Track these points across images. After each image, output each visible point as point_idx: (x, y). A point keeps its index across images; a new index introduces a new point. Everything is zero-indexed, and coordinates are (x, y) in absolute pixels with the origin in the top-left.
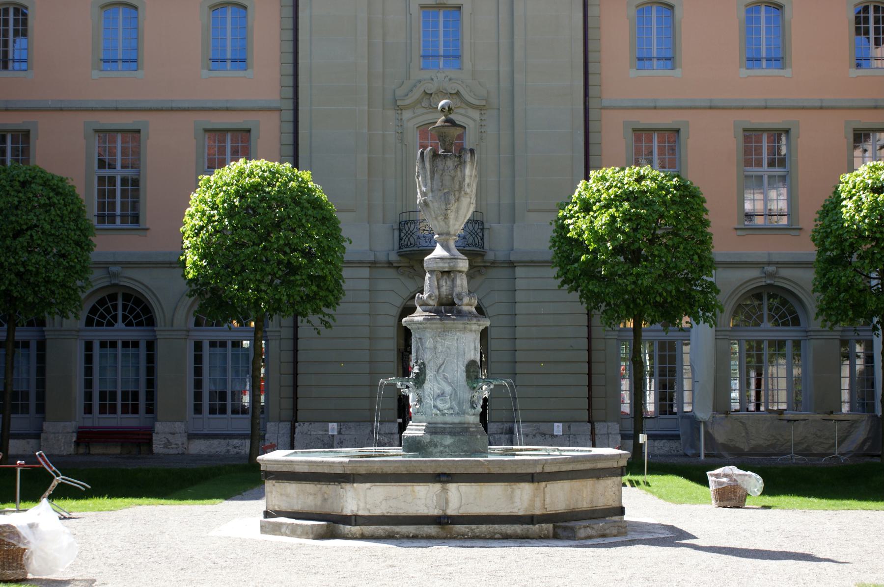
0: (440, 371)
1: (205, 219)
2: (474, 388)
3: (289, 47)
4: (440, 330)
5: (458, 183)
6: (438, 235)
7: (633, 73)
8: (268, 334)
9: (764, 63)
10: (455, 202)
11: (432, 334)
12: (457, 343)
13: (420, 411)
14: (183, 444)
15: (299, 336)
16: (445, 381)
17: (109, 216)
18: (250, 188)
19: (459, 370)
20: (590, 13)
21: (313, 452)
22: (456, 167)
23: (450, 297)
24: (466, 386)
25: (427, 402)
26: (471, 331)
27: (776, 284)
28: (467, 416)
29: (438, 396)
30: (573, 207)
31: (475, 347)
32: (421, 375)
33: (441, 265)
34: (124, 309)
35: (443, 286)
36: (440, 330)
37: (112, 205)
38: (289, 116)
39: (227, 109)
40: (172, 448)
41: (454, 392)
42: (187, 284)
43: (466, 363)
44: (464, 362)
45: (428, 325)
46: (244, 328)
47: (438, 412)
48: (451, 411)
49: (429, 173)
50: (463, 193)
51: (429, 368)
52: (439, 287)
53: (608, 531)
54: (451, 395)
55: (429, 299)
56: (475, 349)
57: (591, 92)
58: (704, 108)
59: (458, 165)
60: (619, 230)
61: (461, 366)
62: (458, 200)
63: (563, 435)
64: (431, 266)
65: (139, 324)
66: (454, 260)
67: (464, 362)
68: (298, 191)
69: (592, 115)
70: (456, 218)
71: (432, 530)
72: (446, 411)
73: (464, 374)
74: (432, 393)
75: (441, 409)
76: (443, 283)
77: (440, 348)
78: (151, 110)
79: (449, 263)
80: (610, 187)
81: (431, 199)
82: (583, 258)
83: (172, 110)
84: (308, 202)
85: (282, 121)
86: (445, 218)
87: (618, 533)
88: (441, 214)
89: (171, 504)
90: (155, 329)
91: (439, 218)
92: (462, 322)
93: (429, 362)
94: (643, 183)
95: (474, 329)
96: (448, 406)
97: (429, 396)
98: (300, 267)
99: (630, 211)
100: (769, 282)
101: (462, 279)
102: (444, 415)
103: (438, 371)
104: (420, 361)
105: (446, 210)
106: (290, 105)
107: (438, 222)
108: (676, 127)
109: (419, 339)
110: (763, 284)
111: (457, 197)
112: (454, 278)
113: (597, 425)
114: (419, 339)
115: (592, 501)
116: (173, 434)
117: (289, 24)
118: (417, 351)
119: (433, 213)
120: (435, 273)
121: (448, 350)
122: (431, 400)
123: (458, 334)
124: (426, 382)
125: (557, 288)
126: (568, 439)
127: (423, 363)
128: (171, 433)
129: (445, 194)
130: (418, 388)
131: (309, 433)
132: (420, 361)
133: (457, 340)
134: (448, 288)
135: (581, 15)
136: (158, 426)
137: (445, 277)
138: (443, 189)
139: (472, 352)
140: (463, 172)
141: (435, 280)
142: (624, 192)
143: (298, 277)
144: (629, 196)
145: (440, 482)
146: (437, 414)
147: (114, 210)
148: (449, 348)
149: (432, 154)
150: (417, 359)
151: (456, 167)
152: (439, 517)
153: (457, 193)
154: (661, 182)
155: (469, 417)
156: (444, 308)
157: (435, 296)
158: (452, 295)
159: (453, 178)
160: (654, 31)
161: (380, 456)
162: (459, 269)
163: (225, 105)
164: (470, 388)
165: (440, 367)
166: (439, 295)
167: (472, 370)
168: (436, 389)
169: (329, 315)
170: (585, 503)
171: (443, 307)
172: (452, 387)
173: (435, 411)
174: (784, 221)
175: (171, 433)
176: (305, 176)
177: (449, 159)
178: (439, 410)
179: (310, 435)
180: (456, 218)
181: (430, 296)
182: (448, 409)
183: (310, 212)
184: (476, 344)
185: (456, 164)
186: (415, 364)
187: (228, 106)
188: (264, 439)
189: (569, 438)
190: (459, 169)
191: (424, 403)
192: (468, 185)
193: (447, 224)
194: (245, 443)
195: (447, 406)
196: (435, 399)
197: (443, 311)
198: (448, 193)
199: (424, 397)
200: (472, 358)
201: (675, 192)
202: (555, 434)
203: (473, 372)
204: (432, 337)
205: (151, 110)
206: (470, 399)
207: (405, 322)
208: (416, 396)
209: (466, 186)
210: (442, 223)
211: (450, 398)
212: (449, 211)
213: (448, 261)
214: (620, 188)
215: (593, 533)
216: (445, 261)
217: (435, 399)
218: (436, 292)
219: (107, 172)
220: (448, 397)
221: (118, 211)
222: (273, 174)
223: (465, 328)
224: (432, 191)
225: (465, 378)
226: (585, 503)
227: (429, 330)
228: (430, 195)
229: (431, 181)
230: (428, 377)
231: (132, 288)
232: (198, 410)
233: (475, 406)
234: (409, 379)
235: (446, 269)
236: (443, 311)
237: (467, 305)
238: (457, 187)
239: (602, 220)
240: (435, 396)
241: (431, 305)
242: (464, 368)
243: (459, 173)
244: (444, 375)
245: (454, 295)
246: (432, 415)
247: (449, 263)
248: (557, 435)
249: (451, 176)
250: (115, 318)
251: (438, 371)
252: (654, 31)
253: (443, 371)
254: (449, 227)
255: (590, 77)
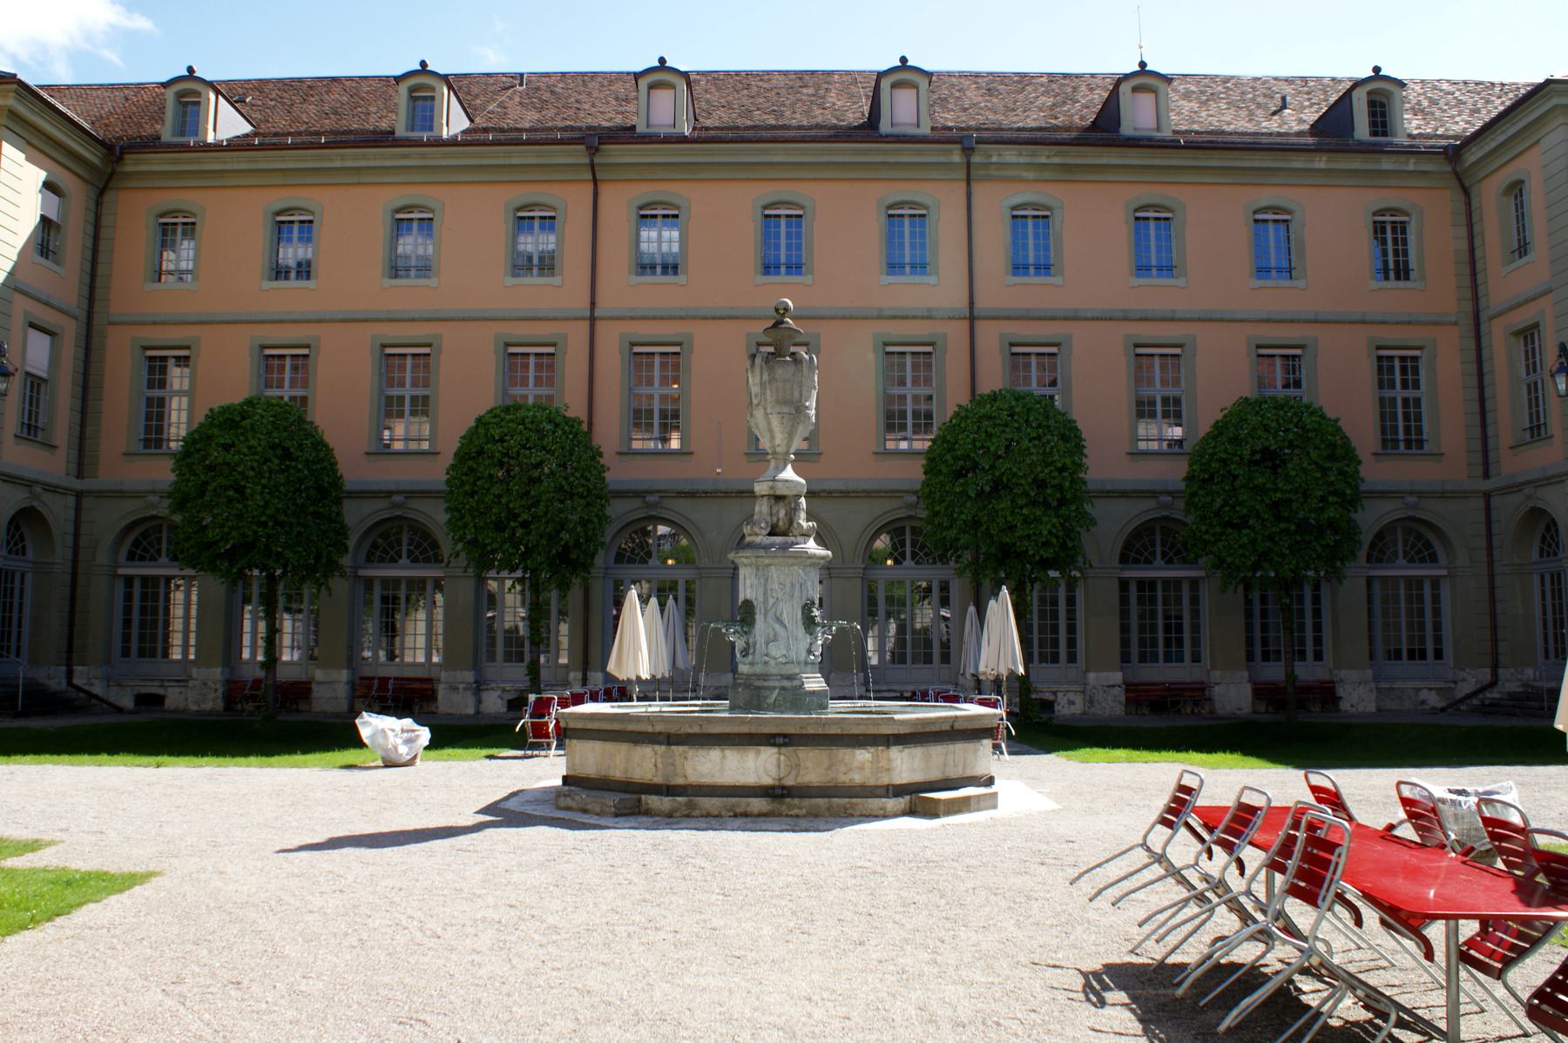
9: (1154, 272)
17: (1417, 441)
21: (922, 706)
27: (405, 515)
34: (1405, 545)
37: (1395, 430)
46: (899, 566)
53: (589, 807)
58: (923, 318)
71: (758, 804)
87: (602, 811)
89: (201, 766)
100: (1164, 514)
108: (932, 340)
110: (1158, 516)
115: (626, 771)
145: (774, 745)
147: (1397, 434)
152: (773, 787)
160: (907, 235)
161: (879, 713)
163: (531, 314)
170: (618, 772)
174: (425, 446)
215: (574, 805)
219: (897, 391)
221: (1401, 436)
226: (618, 772)
250: (1153, 554)
252: (907, 235)
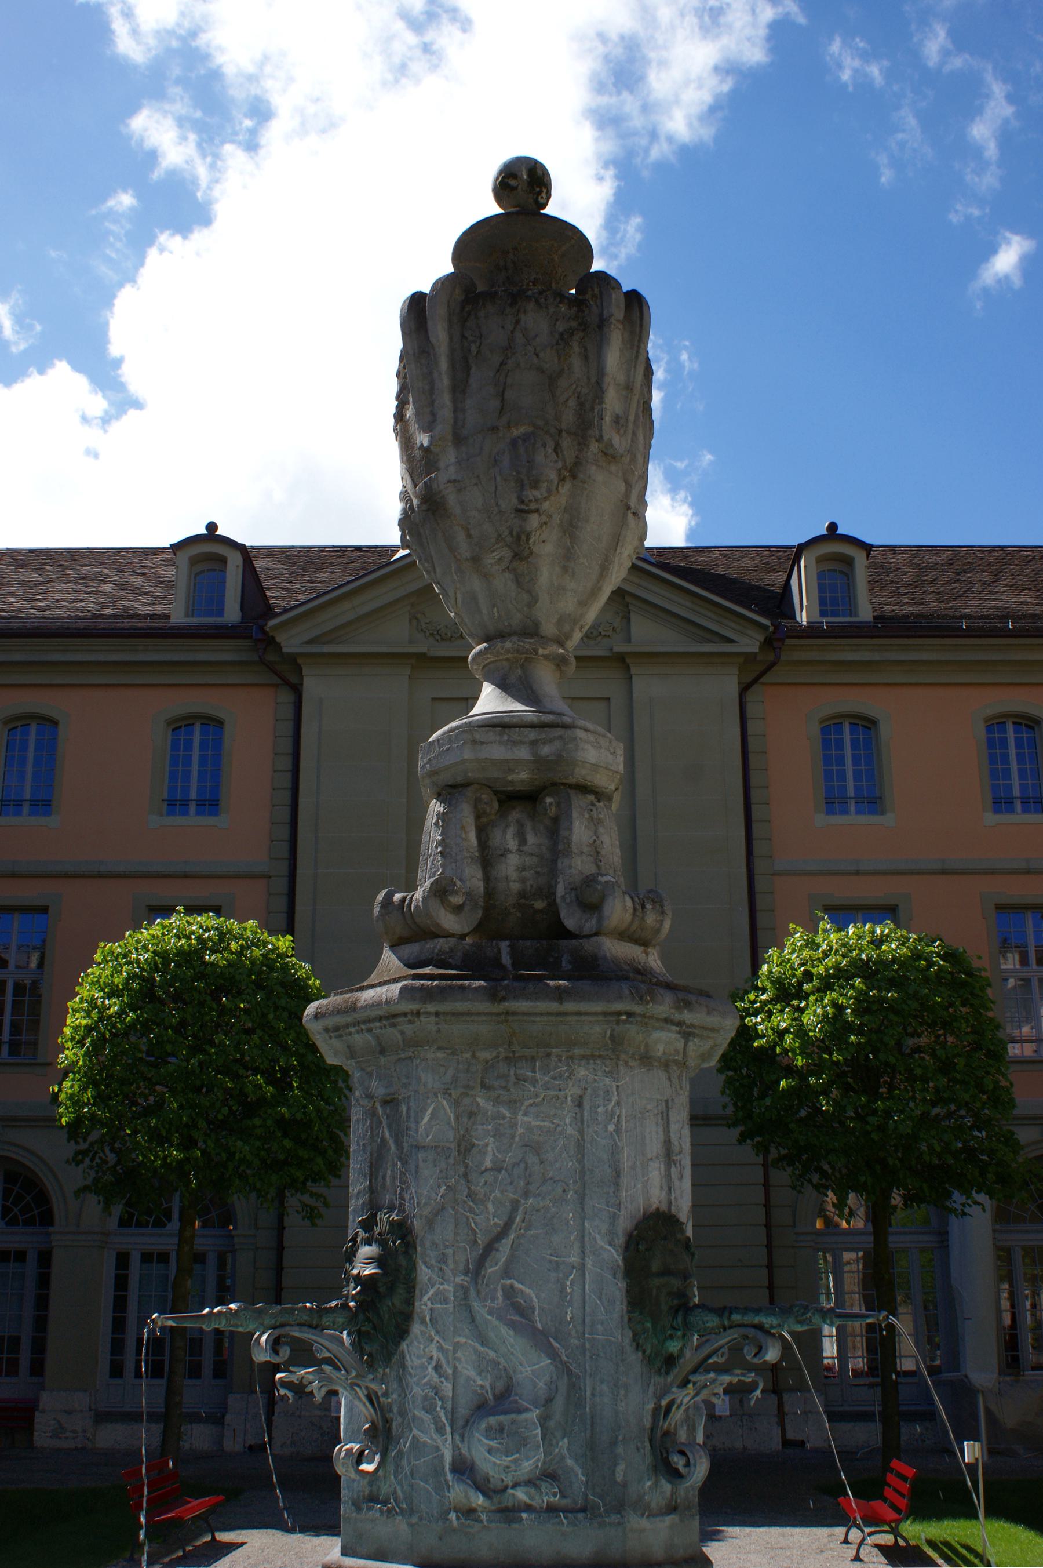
0: (492, 1269)
1: (95, 1014)
2: (670, 1361)
3: (286, 780)
4: (486, 1055)
5: (572, 403)
6: (487, 639)
7: (821, 819)
8: (236, 1240)
10: (562, 479)
11: (451, 1072)
12: (580, 1122)
13: (385, 1489)
14: (85, 1431)
15: (286, 1244)
16: (512, 1325)
18: (176, 955)
19: (589, 1263)
20: (750, 731)
22: (563, 339)
23: (539, 905)
24: (629, 1349)
25: (416, 1443)
26: (646, 1059)
28: (636, 1522)
29: (481, 1408)
30: (757, 996)
31: (668, 1143)
32: (391, 1289)
33: (497, 752)
35: (505, 853)
36: (486, 1055)
38: (281, 885)
39: (186, 876)
40: (66, 1438)
41: (563, 1385)
42: (69, 1141)
43: (625, 1224)
44: (614, 1218)
45: (429, 1024)
47: (479, 1500)
48: (548, 1495)
49: (444, 365)
50: (594, 447)
51: (433, 1254)
52: (487, 858)
54: (549, 1400)
55: (435, 905)
56: (669, 1155)
57: (758, 848)
59: (571, 332)
60: (849, 1028)
61: (601, 1242)
62: (573, 472)
63: (731, 1415)
64: (449, 760)
65: (29, 1222)
66: (559, 732)
67: (614, 1218)
68: (262, 964)
69: (760, 885)
70: (567, 558)
72: (521, 1495)
73: (617, 1288)
74: (447, 1388)
75: (495, 1483)
76: (506, 838)
77: (489, 1150)
78: (66, 876)
79: (534, 743)
80: (826, 955)
81: (452, 473)
82: (783, 1083)
83: (100, 876)
84: (283, 984)
85: (270, 894)
86: (517, 556)
88: (499, 538)
90: (51, 1229)
91: (490, 560)
92: (598, 1007)
93: (430, 1223)
94: (884, 948)
95: (660, 1050)
96: (528, 1466)
97: (430, 1410)
98: (262, 1101)
99: (866, 994)
101: (595, 823)
102: (509, 1513)
103: (476, 1270)
104: (383, 1219)
105: (522, 512)
106: (283, 868)
107: (486, 576)
109: (385, 1103)
111: (570, 462)
112: (556, 820)
113: (786, 1397)
114: (385, 1103)
116: (69, 1413)
117: (287, 745)
118: (374, 1168)
119: (461, 536)
120: (470, 792)
121: (532, 1159)
122: (440, 1430)
123: (581, 1072)
124: (416, 1328)
125: (736, 1142)
126: (739, 1423)
127: (402, 1230)
128: (65, 1412)
129: (514, 443)
130: (371, 1365)
131: (298, 1413)
132: (383, 1219)
133: (580, 1105)
134: (528, 861)
135: (737, 731)
136: (46, 1399)
137: (515, 815)
138: (508, 426)
139: (655, 1173)
140: (594, 358)
141: (470, 821)
142: (853, 963)
143: (257, 1122)
144: (863, 969)
146: (470, 1512)
148: (536, 1148)
149: (459, 295)
150: (373, 1208)
151: (563, 339)
153: (566, 442)
154: (916, 948)
155: (644, 1523)
156: (513, 951)
157: (469, 894)
158: (549, 893)
159: (552, 381)
160: (849, 761)
162: (581, 774)
164: (649, 1360)
165: (490, 1248)
166: (490, 893)
167: (655, 1266)
168: (468, 1370)
169: (318, 1196)
171: (504, 945)
172: (553, 1355)
173: (459, 1492)
175: (65, 1412)
176: (280, 943)
177: (531, 306)
178: (483, 1486)
179: (300, 1417)
180: (567, 558)
181: (440, 891)
182: (530, 1483)
183: (283, 1002)
184: (674, 1127)
185: (561, 327)
186: (362, 1234)
187: (187, 870)
188: (223, 1423)
189: (742, 1421)
190: (576, 348)
191: (406, 1445)
192: (617, 420)
193: (524, 582)
194: (192, 1429)
195: (527, 1466)
196: (462, 1427)
197: (506, 960)
198: (526, 438)
199: (403, 1413)
200: (656, 1198)
201: (942, 963)
202: (717, 1414)
203: (666, 1272)
204: (446, 1092)
205: (66, 876)
206: (647, 1423)
207: (317, 1016)
208: (365, 1410)
209: (607, 419)
210: (503, 582)
211: (544, 1420)
212: (534, 520)
213: (532, 735)
214: (844, 956)
216: (515, 734)
217: (462, 1427)
218: (473, 878)
220: (534, 1415)
222: (222, 935)
223: (616, 1042)
224: (458, 440)
225: (620, 1306)
227: (431, 1054)
228: (449, 457)
229: (454, 401)
230: (424, 1304)
231: (11, 1159)
232: (116, 1371)
233: (678, 1462)
234: (322, 1312)
235: (522, 777)
236: (506, 960)
237: (625, 935)
238: (569, 417)
239: (813, 1015)
240: (463, 1411)
241: (448, 935)
242: (616, 1256)
243: (576, 362)
244: (510, 1293)
245: (560, 890)
246: (444, 1516)
247: (534, 743)
248: (720, 1417)
249: (541, 370)
251: (476, 1270)
252: (849, 761)
253: (507, 1273)
254: (534, 600)
255: (755, 826)
